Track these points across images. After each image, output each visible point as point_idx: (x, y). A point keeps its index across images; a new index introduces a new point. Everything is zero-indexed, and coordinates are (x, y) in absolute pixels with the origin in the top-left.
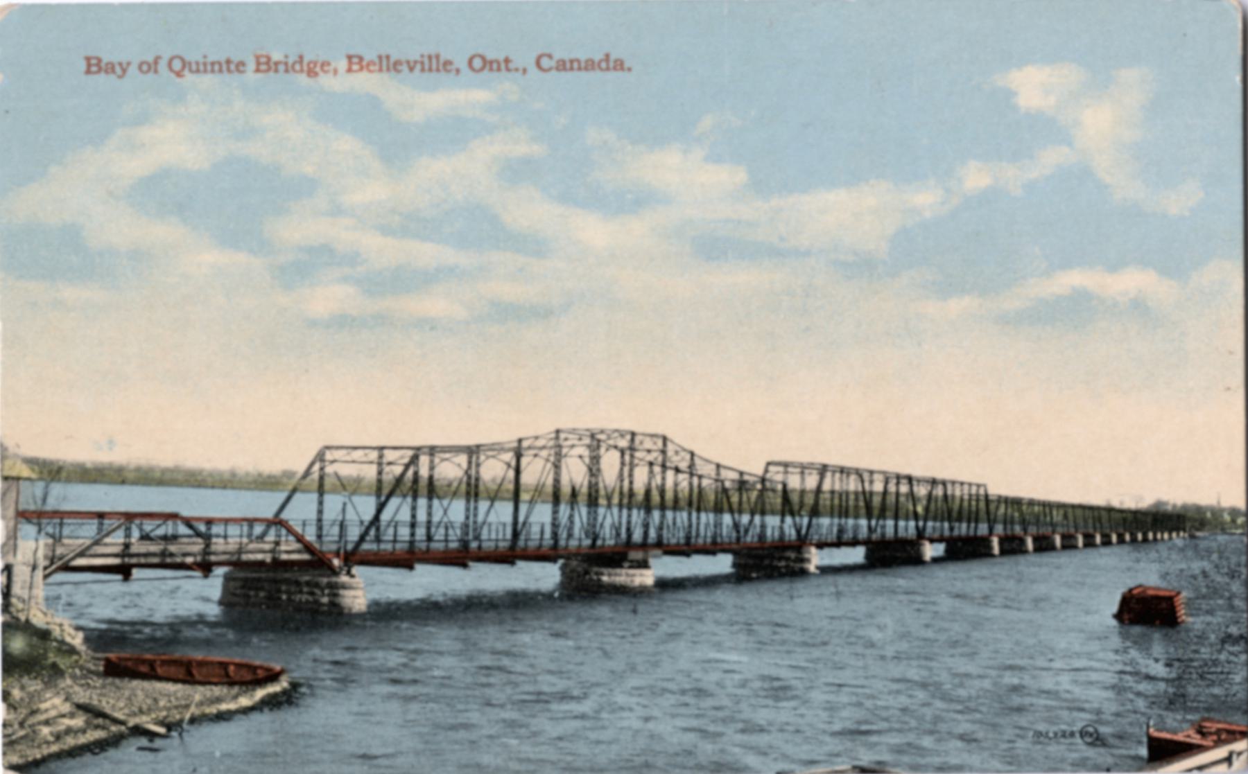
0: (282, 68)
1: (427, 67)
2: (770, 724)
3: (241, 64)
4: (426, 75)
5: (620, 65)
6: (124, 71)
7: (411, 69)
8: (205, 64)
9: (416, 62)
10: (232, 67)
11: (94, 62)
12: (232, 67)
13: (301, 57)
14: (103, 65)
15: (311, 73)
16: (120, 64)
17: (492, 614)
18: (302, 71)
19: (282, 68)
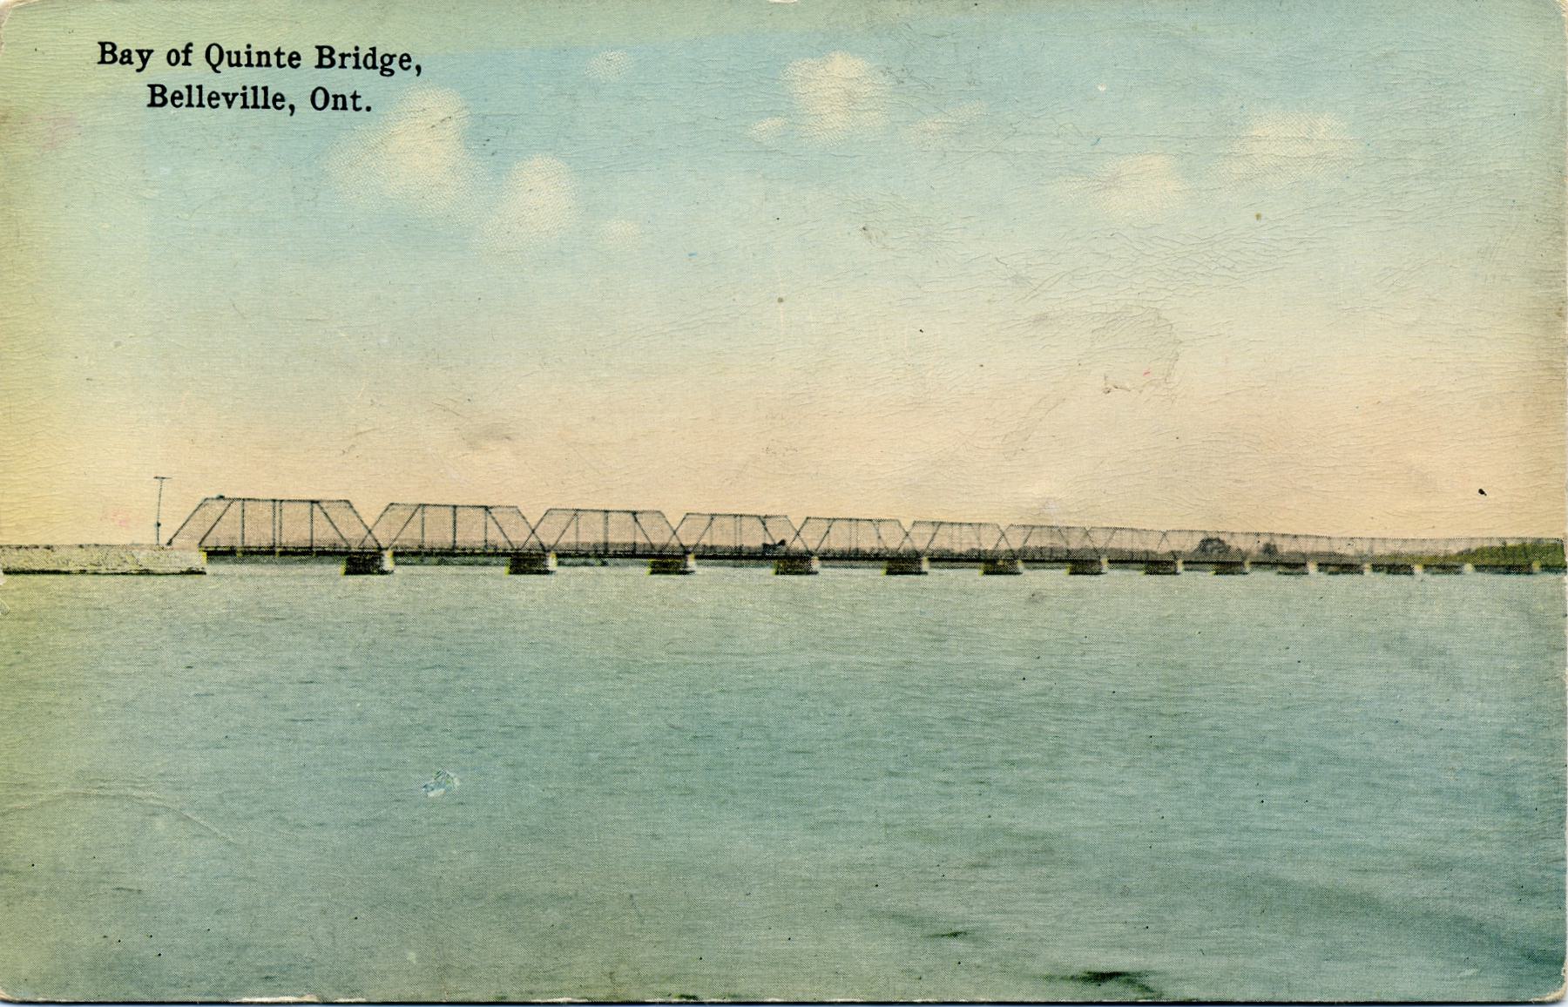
0: (350, 62)
1: (250, 102)
2: (1362, 557)
3: (294, 59)
4: (339, 113)
5: (7, 572)
6: (144, 61)
7: (230, 104)
8: (249, 54)
9: (235, 95)
10: (284, 60)
11: (108, 48)
12: (284, 60)
13: (374, 49)
14: (118, 53)
15: (386, 71)
16: (140, 52)
17: (865, 563)
18: (374, 67)
19: (350, 62)
